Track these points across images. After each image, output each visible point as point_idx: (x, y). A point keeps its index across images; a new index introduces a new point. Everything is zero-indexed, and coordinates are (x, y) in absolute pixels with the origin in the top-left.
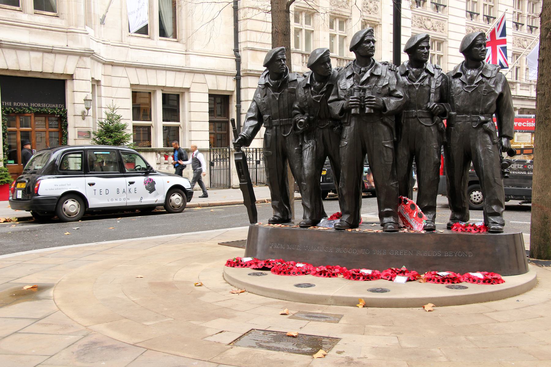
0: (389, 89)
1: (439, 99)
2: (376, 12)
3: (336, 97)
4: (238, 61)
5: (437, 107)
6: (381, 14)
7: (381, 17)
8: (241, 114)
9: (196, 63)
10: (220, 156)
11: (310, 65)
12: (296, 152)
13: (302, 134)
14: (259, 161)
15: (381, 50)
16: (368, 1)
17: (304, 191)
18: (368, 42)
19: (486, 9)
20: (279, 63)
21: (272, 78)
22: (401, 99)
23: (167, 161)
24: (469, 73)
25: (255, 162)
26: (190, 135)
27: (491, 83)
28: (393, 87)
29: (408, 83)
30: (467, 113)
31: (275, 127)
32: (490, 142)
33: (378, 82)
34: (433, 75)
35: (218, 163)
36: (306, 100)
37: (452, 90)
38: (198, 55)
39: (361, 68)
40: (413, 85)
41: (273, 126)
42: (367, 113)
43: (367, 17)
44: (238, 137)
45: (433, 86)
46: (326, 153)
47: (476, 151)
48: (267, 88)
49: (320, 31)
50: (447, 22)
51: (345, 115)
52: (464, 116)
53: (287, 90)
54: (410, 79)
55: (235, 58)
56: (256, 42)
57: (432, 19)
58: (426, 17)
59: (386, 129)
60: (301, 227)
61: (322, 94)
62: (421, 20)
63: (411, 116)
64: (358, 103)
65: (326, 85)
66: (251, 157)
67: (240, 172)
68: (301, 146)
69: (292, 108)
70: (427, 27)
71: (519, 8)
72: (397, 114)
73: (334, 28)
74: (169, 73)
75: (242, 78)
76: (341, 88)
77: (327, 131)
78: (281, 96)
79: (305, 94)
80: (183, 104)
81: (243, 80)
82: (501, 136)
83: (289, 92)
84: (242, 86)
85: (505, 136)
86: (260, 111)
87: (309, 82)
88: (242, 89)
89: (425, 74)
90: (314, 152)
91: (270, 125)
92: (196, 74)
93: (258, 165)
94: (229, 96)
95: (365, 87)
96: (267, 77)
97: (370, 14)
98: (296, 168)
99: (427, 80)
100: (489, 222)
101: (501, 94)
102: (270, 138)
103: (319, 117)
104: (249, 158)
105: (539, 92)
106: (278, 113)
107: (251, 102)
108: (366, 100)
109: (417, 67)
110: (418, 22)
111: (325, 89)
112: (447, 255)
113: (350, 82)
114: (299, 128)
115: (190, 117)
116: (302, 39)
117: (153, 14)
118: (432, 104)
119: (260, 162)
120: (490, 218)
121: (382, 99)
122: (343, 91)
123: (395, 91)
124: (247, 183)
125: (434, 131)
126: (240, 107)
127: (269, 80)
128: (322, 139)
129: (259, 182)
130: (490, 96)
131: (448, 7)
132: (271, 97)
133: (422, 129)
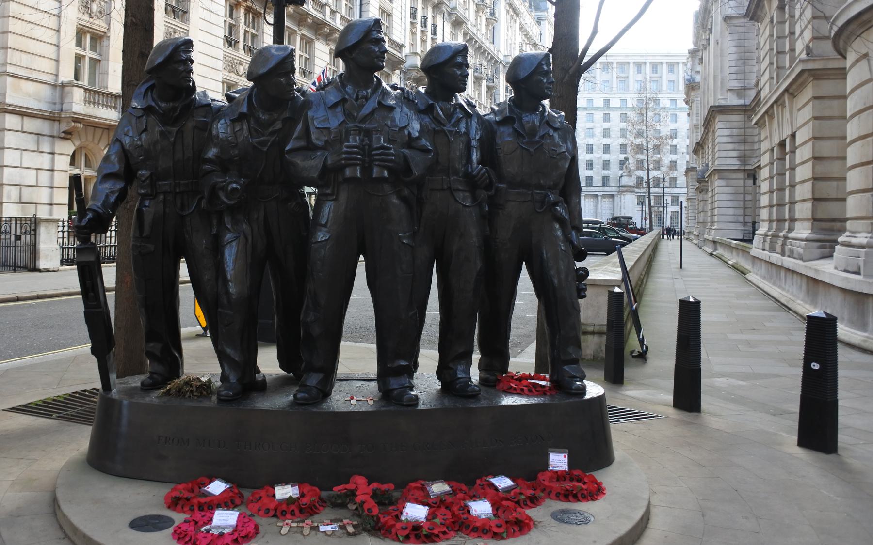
0: (410, 133)
3: (302, 143)
5: (484, 173)
14: (20, 236)
20: (181, 68)
25: (13, 238)
42: (375, 178)
44: (87, 215)
57: (244, 64)
58: (238, 60)
62: (231, 63)
66: (8, 229)
69: (199, 157)
79: (235, 133)
87: (244, 109)
93: (18, 242)
96: (149, 93)
108: (374, 152)
111: (278, 125)
114: (225, 200)
116: (84, 68)
120: (566, 367)
122: (322, 132)
127: (153, 100)
129: (9, 264)
132: (157, 136)
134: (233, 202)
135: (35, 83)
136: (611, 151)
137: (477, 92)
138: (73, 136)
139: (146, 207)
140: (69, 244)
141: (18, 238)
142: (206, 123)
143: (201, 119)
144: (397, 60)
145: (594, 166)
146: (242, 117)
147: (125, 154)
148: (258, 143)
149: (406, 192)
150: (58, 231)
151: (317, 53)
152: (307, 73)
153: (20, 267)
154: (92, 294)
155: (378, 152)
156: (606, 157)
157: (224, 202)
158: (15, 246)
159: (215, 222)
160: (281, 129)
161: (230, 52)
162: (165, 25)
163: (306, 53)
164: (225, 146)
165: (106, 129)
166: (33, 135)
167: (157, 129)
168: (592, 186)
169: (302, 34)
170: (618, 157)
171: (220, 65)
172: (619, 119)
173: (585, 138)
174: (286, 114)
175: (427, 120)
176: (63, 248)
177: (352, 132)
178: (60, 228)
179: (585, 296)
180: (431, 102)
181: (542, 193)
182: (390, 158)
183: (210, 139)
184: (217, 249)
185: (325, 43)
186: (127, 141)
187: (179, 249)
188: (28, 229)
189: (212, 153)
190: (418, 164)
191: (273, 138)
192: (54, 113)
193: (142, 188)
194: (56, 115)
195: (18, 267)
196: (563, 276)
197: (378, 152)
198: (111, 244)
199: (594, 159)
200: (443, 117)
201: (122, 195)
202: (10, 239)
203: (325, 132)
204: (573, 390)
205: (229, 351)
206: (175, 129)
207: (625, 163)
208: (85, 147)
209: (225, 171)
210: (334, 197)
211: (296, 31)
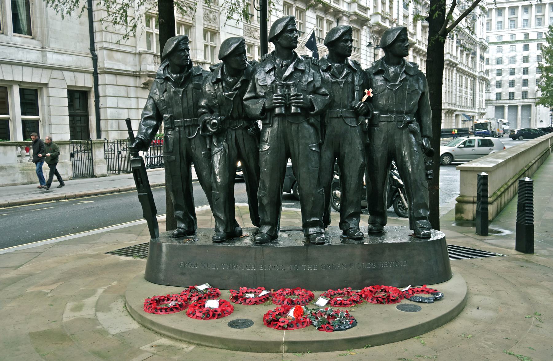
0: (314, 85)
3: (253, 94)
4: (95, 59)
9: (52, 59)
10: (81, 148)
11: (222, 57)
12: (204, 157)
14: (121, 152)
16: (142, 0)
17: (217, 200)
18: (183, 50)
20: (183, 54)
23: (28, 154)
25: (116, 153)
26: (50, 128)
29: (331, 79)
33: (301, 77)
35: (83, 154)
36: (216, 97)
38: (55, 52)
39: (282, 62)
40: (337, 82)
41: (175, 127)
43: (207, 25)
45: (356, 83)
46: (288, 155)
48: (167, 83)
51: (267, 115)
53: (191, 86)
54: (333, 75)
55: (92, 56)
59: (312, 130)
60: (215, 242)
61: (235, 90)
63: (335, 116)
65: (240, 80)
66: (113, 148)
67: (139, 180)
68: (210, 150)
69: (197, 106)
72: (322, 114)
74: (25, 69)
75: (99, 75)
76: (261, 84)
77: (240, 132)
78: (185, 93)
79: (215, 90)
80: (42, 99)
81: (100, 77)
83: (194, 88)
84: (100, 82)
86: (160, 110)
90: (226, 157)
91: (171, 126)
92: (53, 70)
94: (87, 91)
103: (232, 117)
106: (182, 112)
107: (145, 101)
108: (291, 98)
109: (339, 62)
111: (239, 85)
112: (381, 266)
113: (270, 78)
114: (211, 130)
115: (49, 111)
117: (5, 10)
122: (263, 88)
123: (320, 88)
124: (147, 193)
128: (234, 141)
132: (172, 94)
134: (214, 131)
135: (122, 53)
136: (529, 73)
137: (424, 37)
139: (169, 135)
142: (200, 85)
144: (363, 19)
145: (515, 84)
146: (218, 81)
147: (156, 106)
149: (312, 120)
151: (308, 19)
154: (142, 185)
156: (525, 77)
157: (210, 131)
158: (118, 158)
159: (208, 141)
162: (203, 8)
163: (300, 19)
164: (211, 98)
166: (124, 87)
167: (172, 90)
168: (501, 100)
169: (297, 7)
170: (535, 76)
172: (536, 48)
173: (509, 64)
174: (242, 78)
183: (203, 95)
184: (209, 156)
185: (313, 11)
186: (157, 97)
187: (189, 159)
188: (125, 147)
192: (136, 72)
194: (137, 73)
196: (415, 166)
199: (516, 79)
204: (421, 235)
205: (219, 214)
206: (182, 90)
207: (540, 81)
209: (212, 112)
211: (292, 5)
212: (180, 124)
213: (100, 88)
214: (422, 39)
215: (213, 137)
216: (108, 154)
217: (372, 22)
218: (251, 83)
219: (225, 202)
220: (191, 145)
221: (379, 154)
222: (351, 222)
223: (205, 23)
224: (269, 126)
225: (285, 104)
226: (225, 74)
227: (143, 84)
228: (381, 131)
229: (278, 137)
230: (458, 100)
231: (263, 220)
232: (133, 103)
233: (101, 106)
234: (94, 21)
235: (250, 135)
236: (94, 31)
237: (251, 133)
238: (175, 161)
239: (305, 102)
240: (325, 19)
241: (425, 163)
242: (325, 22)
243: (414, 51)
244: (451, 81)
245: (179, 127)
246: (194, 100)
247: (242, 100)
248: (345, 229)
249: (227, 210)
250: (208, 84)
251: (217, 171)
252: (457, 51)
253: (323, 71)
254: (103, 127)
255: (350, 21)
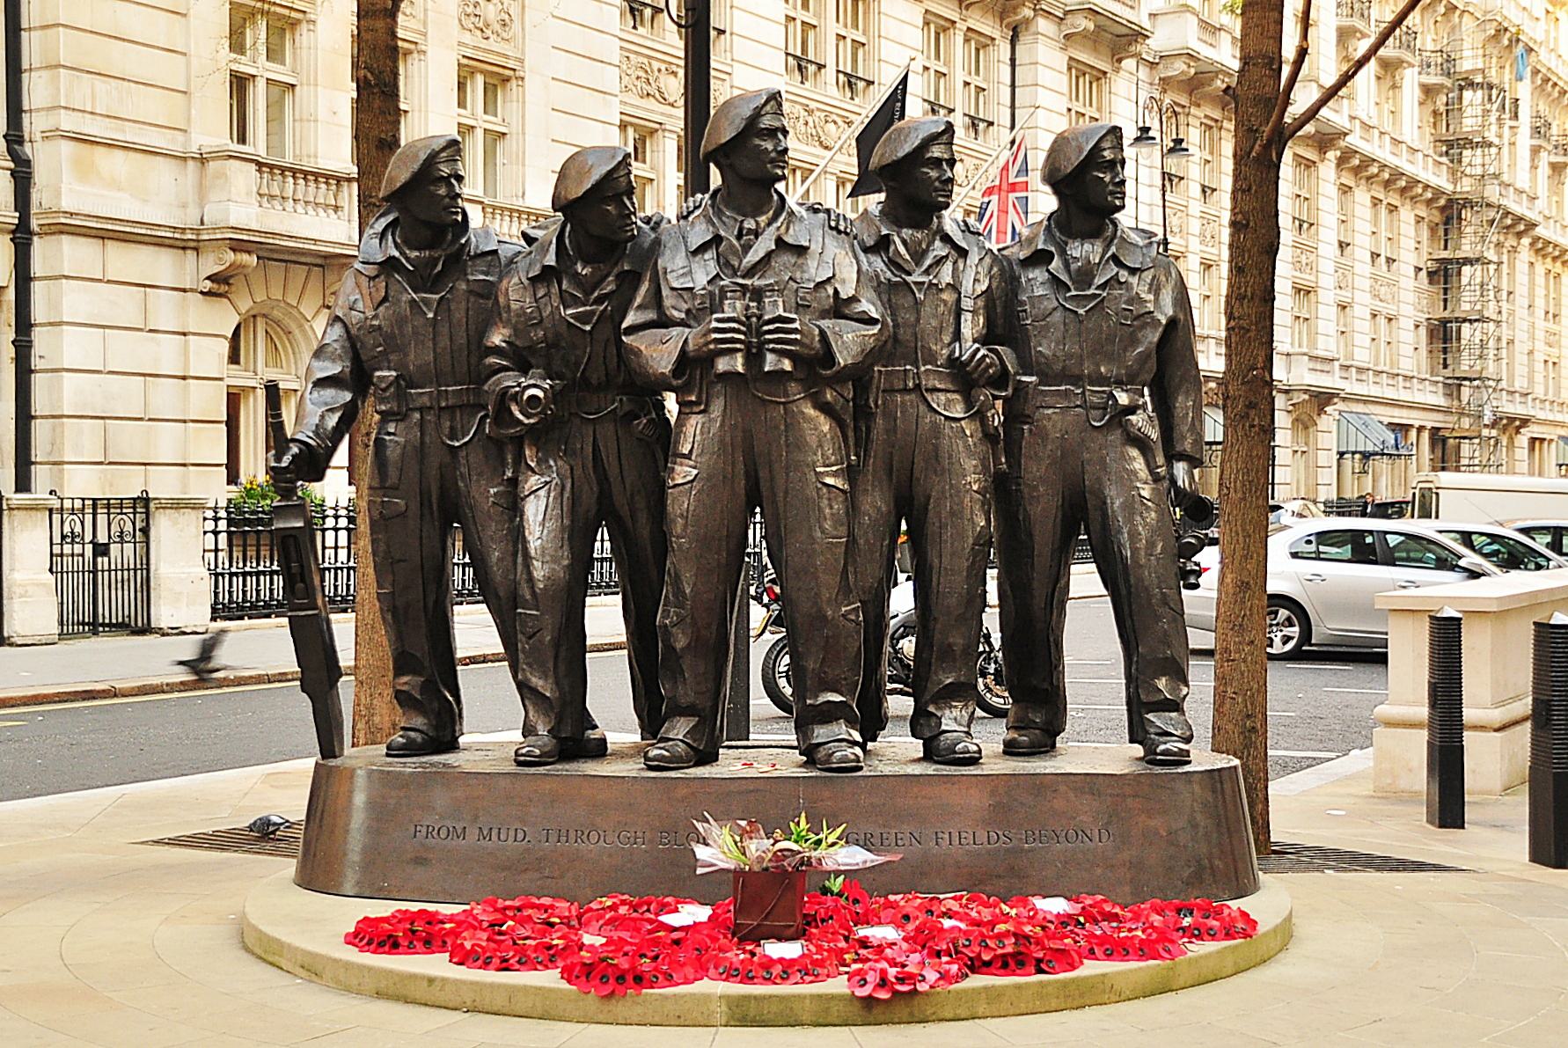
0: (836, 292)
1: (984, 332)
2: (505, 35)
3: (651, 315)
5: (984, 356)
6: (524, 43)
7: (523, 53)
8: (32, 371)
11: (563, 202)
13: (535, 435)
14: (107, 545)
15: (524, 165)
19: (845, 51)
21: (407, 243)
22: (876, 329)
24: (1076, 254)
27: (1140, 286)
28: (847, 291)
30: (1077, 380)
31: (417, 415)
32: (1144, 473)
34: (963, 253)
36: (541, 321)
37: (1023, 303)
39: (742, 222)
43: (475, 48)
44: (289, 448)
45: (967, 286)
46: (754, 498)
47: (1103, 504)
48: (389, 276)
49: (319, 88)
50: (727, 84)
52: (1063, 388)
54: (893, 264)
55: (12, 165)
56: (92, 113)
59: (825, 425)
60: (519, 764)
61: (599, 301)
64: (742, 337)
65: (615, 271)
66: (78, 529)
68: (514, 482)
70: (666, 96)
71: (938, 57)
72: (859, 375)
73: (288, 60)
75: (35, 239)
76: (675, 285)
77: (608, 431)
81: (38, 246)
82: (1171, 457)
83: (470, 292)
84: (38, 267)
85: (1182, 457)
86: (364, 358)
87: (551, 260)
88: (35, 279)
89: (939, 249)
95: (756, 282)
96: (390, 237)
97: (487, 38)
98: (494, 560)
99: (947, 268)
100: (1147, 732)
101: (1172, 322)
102: (399, 451)
104: (72, 532)
105: (1232, 323)
108: (766, 328)
110: (638, 78)
111: (609, 287)
114: (521, 417)
118: (968, 347)
119: (108, 549)
120: (1150, 716)
121: (819, 327)
123: (854, 299)
125: (972, 436)
126: (30, 347)
127: (397, 246)
130: (1143, 326)
131: (732, 34)
133: (936, 430)
134: (532, 421)
135: (132, 154)
138: (233, 288)
139: (389, 434)
140: (231, 566)
141: (101, 550)
143: (482, 277)
144: (1124, 31)
147: (353, 342)
148: (572, 316)
150: (205, 533)
151: (888, 27)
152: (861, 85)
153: (110, 625)
155: (771, 327)
157: (520, 422)
158: (95, 572)
160: (612, 292)
161: (641, 41)
164: (522, 325)
165: (316, 265)
167: (405, 297)
171: (610, 78)
175: (878, 263)
176: (217, 575)
177: (729, 294)
178: (210, 525)
179: (1196, 586)
180: (884, 232)
181: (1103, 392)
182: (793, 336)
184: (513, 505)
188: (129, 527)
189: (497, 338)
190: (849, 342)
191: (602, 308)
193: (382, 401)
195: (103, 625)
197: (771, 327)
198: (339, 565)
200: (908, 257)
201: (349, 417)
202: (83, 555)
203: (686, 295)
205: (537, 682)
206: (437, 297)
208: (264, 316)
210: (702, 407)
212: (426, 400)
213: (37, 289)
214: (1380, 115)
215: (527, 442)
216: (62, 555)
217: (1159, 41)
218: (647, 283)
219: (556, 644)
220: (455, 468)
221: (1043, 508)
222: (947, 712)
223: (467, 38)
224: (696, 409)
225: (748, 345)
226: (569, 255)
227: (208, 278)
228: (1042, 434)
229: (722, 441)
230: (1539, 378)
231: (672, 699)
232: (165, 352)
233: (36, 363)
234: (24, 25)
235: (640, 440)
236: (25, 65)
237: (641, 432)
238: (403, 515)
239: (806, 341)
240: (961, 26)
241: (1178, 538)
242: (960, 38)
243: (1341, 162)
244: (1510, 293)
245: (421, 410)
246: (472, 327)
247: (618, 333)
248: (928, 735)
249: (562, 668)
250: (515, 280)
251: (534, 544)
252: (1534, 167)
253: (866, 250)
254: (39, 451)
255: (1067, 37)
